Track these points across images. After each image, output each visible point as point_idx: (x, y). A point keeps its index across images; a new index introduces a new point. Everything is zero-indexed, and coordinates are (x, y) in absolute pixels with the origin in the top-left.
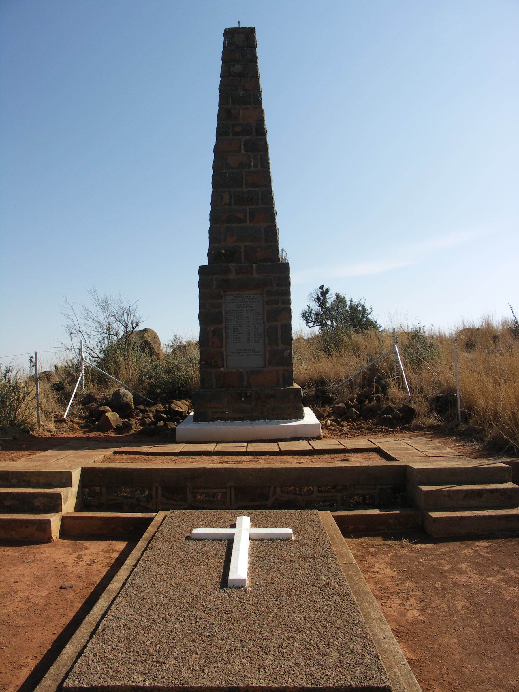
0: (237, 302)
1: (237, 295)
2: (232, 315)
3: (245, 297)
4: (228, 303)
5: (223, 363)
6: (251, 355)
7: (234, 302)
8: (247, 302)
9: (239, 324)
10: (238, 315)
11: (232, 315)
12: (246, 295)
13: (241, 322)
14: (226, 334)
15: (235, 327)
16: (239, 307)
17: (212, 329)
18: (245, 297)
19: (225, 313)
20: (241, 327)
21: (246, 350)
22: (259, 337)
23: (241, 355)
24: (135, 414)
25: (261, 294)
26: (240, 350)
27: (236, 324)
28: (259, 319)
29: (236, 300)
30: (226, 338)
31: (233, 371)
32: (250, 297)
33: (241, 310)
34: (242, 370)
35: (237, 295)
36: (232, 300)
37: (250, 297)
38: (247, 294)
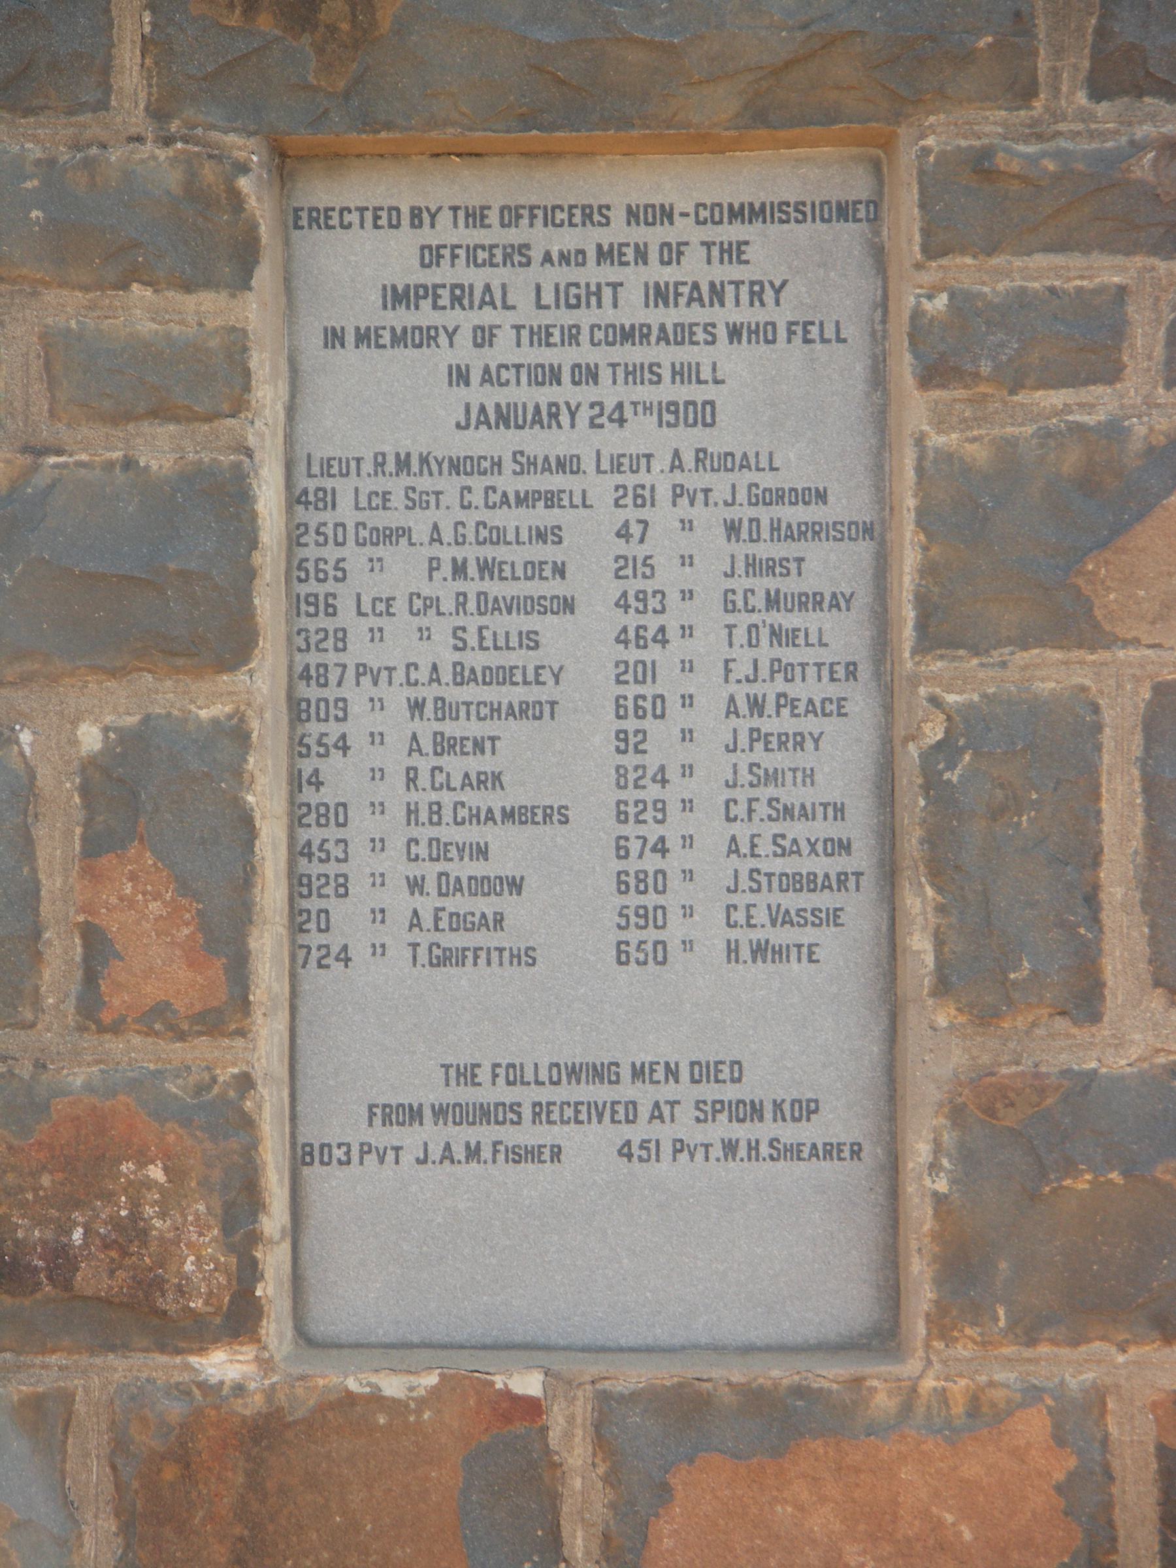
0: (484, 337)
1: (476, 217)
2: (391, 535)
3: (604, 255)
4: (334, 338)
5: (249, 1272)
6: (679, 1147)
7: (427, 337)
8: (627, 335)
9: (504, 675)
10: (498, 537)
11: (391, 535)
12: (619, 232)
13: (531, 640)
14: (297, 817)
15: (446, 711)
16: (505, 418)
17: (90, 738)
18: (604, 255)
19: (295, 499)
20: (522, 711)
21: (600, 1073)
22: (810, 883)
23: (518, 1155)
24: (1009, 1064)
25: (844, 212)
26: (514, 1075)
27: (462, 676)
28: (811, 601)
29: (460, 296)
30: (298, 885)
31: (393, 1386)
32: (673, 253)
33: (527, 464)
34: (529, 1384)
35: (476, 217)
36: (398, 297)
37: (673, 253)
38: (632, 215)
